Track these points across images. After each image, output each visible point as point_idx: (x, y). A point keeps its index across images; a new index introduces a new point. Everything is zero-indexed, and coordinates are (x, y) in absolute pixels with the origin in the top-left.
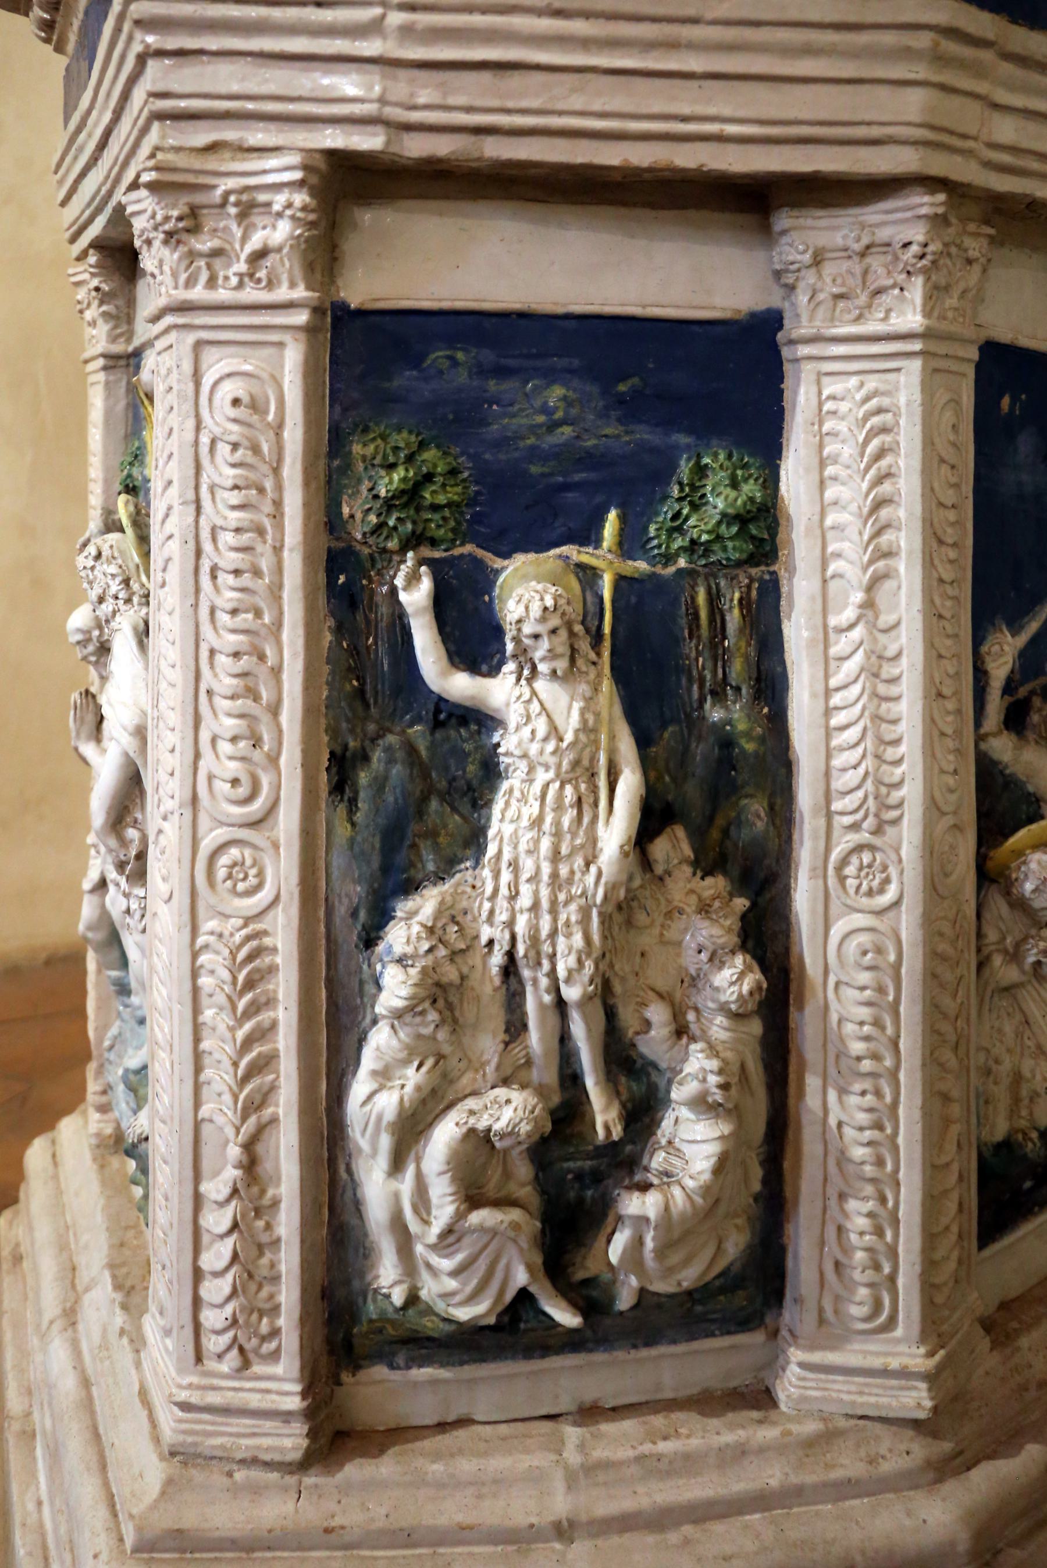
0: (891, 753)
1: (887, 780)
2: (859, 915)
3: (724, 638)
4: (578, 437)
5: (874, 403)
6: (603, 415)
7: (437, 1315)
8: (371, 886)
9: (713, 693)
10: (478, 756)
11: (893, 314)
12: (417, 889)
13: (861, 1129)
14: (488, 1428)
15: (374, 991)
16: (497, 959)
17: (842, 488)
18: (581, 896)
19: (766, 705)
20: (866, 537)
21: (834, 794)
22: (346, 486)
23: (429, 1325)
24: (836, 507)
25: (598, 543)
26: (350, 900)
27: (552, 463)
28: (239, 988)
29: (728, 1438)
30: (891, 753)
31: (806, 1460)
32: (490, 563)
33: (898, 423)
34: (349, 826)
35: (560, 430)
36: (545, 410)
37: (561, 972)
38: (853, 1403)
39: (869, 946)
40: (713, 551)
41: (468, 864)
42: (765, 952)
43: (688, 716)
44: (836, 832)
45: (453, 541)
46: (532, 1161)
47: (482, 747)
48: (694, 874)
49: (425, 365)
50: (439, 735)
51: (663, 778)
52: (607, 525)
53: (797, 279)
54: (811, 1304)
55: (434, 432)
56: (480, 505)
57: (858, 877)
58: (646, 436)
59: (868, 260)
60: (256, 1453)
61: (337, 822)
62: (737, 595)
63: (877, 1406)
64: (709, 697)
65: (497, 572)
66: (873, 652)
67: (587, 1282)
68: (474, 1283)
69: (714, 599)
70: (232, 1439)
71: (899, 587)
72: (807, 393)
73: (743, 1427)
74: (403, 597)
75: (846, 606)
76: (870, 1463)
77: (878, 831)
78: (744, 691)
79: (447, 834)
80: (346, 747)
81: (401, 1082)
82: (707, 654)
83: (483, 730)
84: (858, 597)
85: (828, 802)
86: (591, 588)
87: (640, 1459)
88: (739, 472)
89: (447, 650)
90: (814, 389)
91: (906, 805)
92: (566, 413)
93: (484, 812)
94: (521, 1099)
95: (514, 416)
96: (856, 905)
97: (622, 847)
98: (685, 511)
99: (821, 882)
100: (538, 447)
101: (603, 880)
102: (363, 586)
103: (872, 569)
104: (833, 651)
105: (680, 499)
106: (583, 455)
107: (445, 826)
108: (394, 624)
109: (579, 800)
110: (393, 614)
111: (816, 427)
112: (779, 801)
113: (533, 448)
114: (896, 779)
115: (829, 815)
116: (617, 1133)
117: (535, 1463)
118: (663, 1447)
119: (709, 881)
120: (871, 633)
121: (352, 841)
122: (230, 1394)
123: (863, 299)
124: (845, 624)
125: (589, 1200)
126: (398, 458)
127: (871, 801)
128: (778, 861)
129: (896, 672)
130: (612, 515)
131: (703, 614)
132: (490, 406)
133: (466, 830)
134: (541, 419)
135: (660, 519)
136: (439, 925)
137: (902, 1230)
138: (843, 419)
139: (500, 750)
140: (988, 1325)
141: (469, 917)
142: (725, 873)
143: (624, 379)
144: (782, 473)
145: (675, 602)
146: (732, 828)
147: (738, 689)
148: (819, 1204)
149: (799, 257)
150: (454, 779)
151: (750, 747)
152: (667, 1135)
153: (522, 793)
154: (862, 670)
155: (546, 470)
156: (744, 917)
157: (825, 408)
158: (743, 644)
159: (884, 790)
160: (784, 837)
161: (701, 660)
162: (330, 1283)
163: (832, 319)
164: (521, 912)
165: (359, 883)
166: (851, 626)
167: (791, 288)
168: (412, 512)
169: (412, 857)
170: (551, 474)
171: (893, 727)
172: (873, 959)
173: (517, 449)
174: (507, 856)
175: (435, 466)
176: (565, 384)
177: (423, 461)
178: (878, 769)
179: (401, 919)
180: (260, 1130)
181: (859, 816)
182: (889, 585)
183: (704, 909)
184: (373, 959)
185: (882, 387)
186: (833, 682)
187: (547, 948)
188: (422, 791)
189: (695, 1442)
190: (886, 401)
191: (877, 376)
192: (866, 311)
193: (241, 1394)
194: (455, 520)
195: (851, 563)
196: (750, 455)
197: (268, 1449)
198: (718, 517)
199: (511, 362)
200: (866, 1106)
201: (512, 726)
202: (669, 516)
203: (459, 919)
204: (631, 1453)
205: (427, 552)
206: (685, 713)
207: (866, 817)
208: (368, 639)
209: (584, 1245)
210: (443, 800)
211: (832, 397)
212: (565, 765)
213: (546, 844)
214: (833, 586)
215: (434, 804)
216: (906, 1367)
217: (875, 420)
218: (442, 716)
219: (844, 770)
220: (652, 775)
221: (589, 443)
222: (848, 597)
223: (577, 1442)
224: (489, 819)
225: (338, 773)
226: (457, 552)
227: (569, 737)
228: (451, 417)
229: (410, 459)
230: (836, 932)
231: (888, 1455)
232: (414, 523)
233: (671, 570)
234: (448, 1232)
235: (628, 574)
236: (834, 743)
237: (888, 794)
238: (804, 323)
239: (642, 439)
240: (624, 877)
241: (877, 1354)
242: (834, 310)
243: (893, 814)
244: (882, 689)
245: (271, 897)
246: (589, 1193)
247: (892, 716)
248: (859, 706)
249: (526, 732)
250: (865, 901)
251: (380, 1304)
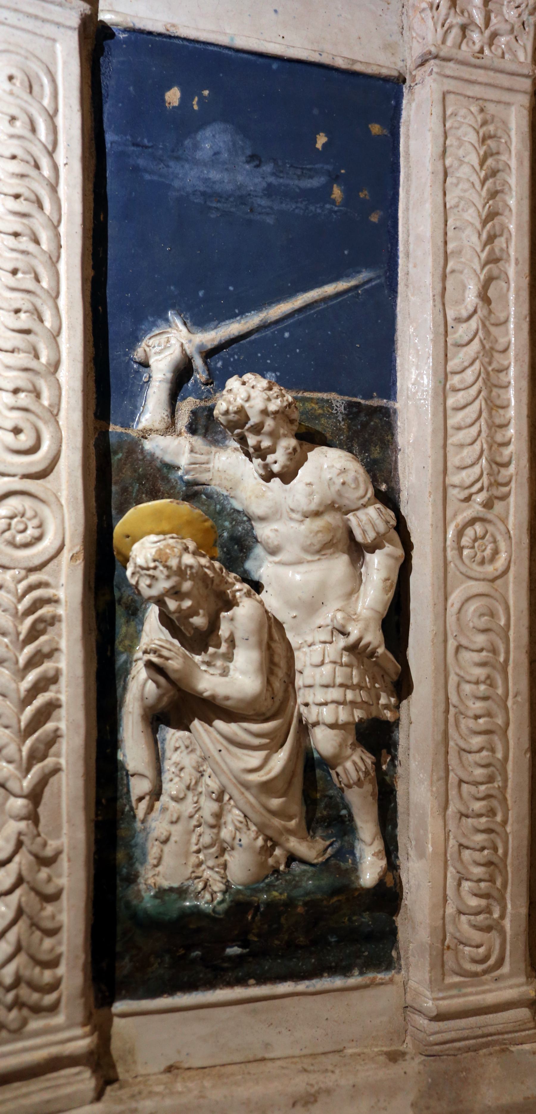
1: (498, 459)
28: (22, 637)
57: (473, 547)
77: (488, 505)
114: (506, 459)
127: (485, 478)
140: (386, 1110)
180: (43, 782)
230: (455, 598)
250: (478, 570)
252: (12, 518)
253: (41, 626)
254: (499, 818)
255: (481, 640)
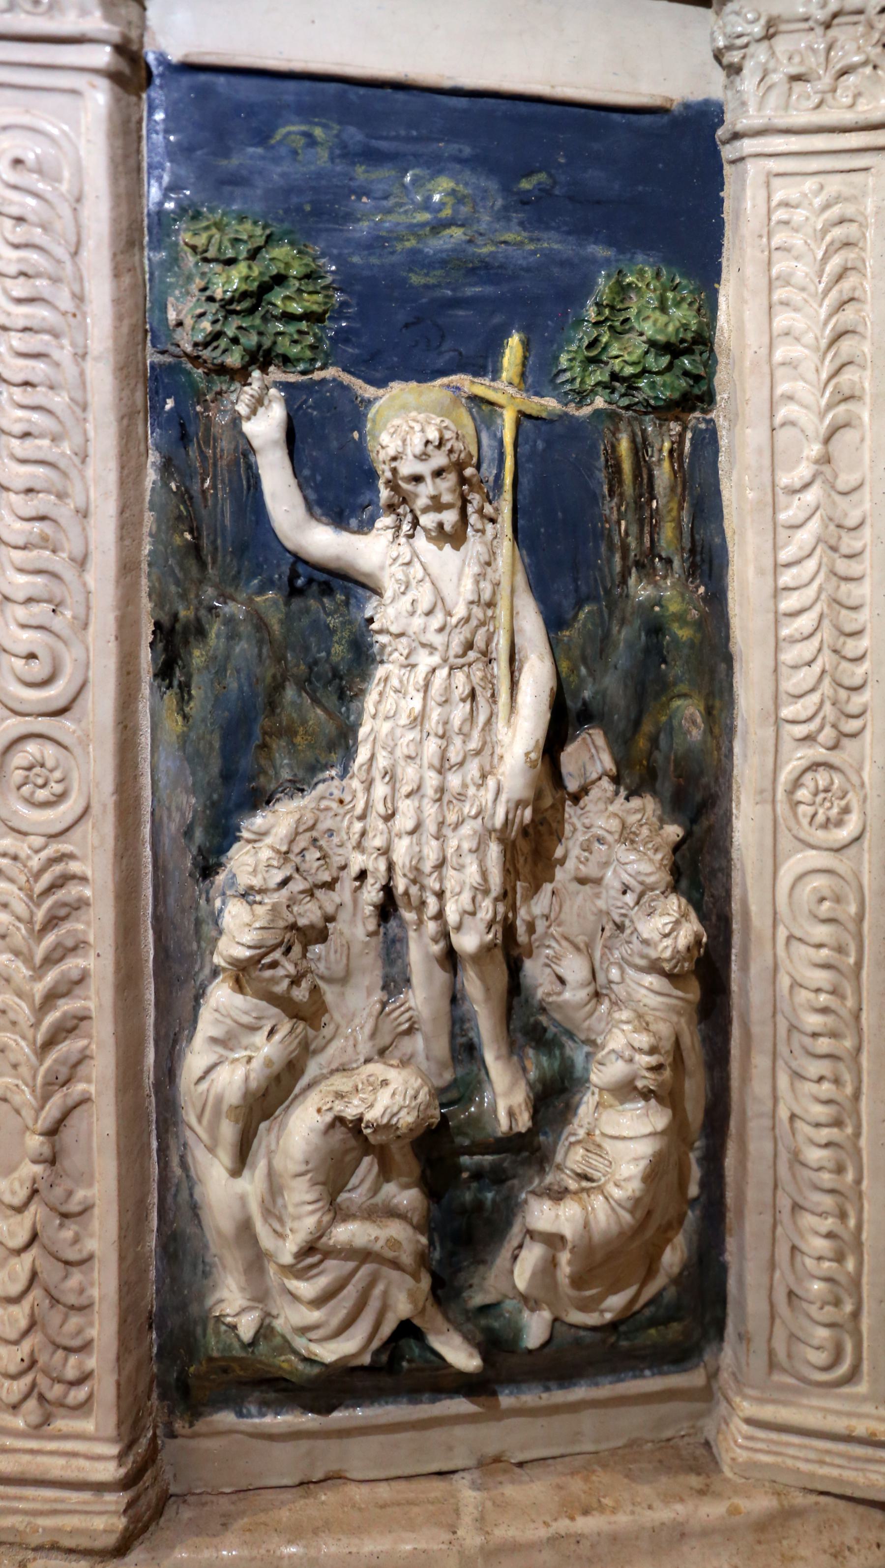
0: (852, 647)
1: (847, 682)
2: (814, 852)
3: (652, 497)
4: (470, 241)
5: (835, 212)
6: (503, 215)
7: (295, 1352)
8: (210, 797)
9: (639, 565)
10: (346, 634)
11: (862, 100)
12: (268, 802)
13: (818, 1125)
14: (365, 1489)
15: (214, 933)
16: (372, 894)
17: (793, 315)
18: (475, 817)
19: (702, 583)
20: (824, 376)
21: (783, 697)
22: (171, 286)
23: (287, 1363)
24: (789, 339)
25: (496, 374)
26: (183, 815)
27: (438, 273)
29: (664, 1514)
30: (852, 647)
31: (758, 1548)
32: (360, 392)
33: (864, 236)
34: (180, 719)
35: (448, 232)
36: (427, 205)
37: (452, 915)
38: (812, 1475)
39: (826, 893)
40: (638, 389)
41: (333, 773)
42: (703, 895)
43: (608, 592)
44: (787, 745)
45: (313, 360)
46: (416, 1155)
47: (350, 622)
48: (617, 793)
49: (273, 142)
50: (297, 603)
51: (579, 670)
52: (507, 351)
53: (744, 58)
54: (759, 1345)
55: (286, 226)
56: (347, 319)
57: (813, 804)
58: (556, 246)
59: (833, 33)
60: (56, 1538)
61: (164, 714)
62: (667, 445)
63: (839, 1481)
64: (634, 570)
65: (369, 403)
66: (831, 519)
67: (485, 1309)
68: (342, 1313)
69: (640, 448)
70: (27, 1519)
71: (862, 440)
72: (754, 198)
73: (682, 1500)
74: (248, 427)
75: (798, 461)
76: (835, 1556)
78: (676, 564)
79: (306, 733)
80: (175, 617)
81: (248, 1053)
82: (630, 515)
83: (353, 601)
84: (815, 449)
85: (777, 707)
86: (488, 428)
87: (555, 1540)
88: (670, 295)
89: (305, 498)
90: (763, 193)
91: (868, 715)
92: (455, 211)
93: (353, 706)
94: (400, 1080)
95: (389, 211)
96: (811, 840)
97: (527, 754)
98: (604, 339)
99: (769, 808)
100: (420, 251)
101: (503, 797)
102: (197, 413)
103: (830, 416)
104: (782, 517)
105: (597, 324)
106: (477, 264)
107: (304, 722)
108: (237, 463)
109: (473, 695)
110: (236, 448)
111: (765, 240)
112: (717, 704)
113: (414, 252)
114: (857, 681)
115: (778, 721)
116: (524, 1122)
117: (423, 1545)
118: (585, 1524)
119: (636, 802)
120: (829, 496)
121: (184, 739)
122: (27, 1458)
123: (827, 80)
124: (798, 484)
125: (489, 1203)
126: (238, 253)
127: (828, 708)
128: (717, 779)
129: (857, 545)
130: (514, 343)
131: (627, 466)
132: (359, 198)
133: (330, 728)
134: (426, 216)
135: (574, 347)
136: (296, 849)
137: (866, 1257)
138: (796, 230)
139: (374, 626)
141: (335, 840)
142: (655, 793)
143: (528, 174)
144: (722, 300)
145: (592, 451)
146: (662, 736)
147: (669, 562)
148: (768, 1218)
149: (748, 29)
150: (316, 662)
151: (684, 633)
152: (585, 1122)
153: (401, 681)
154: (819, 540)
155: (431, 281)
156: (677, 848)
157: (775, 217)
158: (674, 505)
159: (843, 694)
160: (724, 750)
161: (623, 523)
162: (161, 1308)
163: (787, 107)
164: (399, 836)
165: (194, 793)
166: (806, 486)
167: (734, 70)
168: (258, 322)
169: (263, 762)
170: (438, 286)
171: (853, 615)
172: (830, 909)
173: (393, 253)
174: (382, 761)
175: (288, 265)
176: (453, 176)
177: (272, 259)
178: (836, 668)
179: (249, 841)
181: (813, 726)
182: (847, 437)
183: (627, 835)
184: (212, 892)
185: (847, 191)
186: (784, 556)
187: (433, 883)
188: (274, 677)
189: (622, 1519)
190: (849, 210)
191: (839, 177)
192: (829, 96)
193: (41, 1459)
194: (315, 335)
195: (806, 407)
196: (683, 275)
197: (73, 1532)
198: (645, 347)
199: (383, 145)
200: (824, 1096)
201: (388, 594)
202: (586, 343)
203: (322, 842)
204: (543, 1533)
205: (275, 374)
206: (605, 589)
207: (821, 728)
208: (203, 481)
209: (483, 1262)
210: (301, 688)
211: (786, 204)
212: (456, 647)
213: (432, 747)
214: (783, 435)
215: (290, 693)
216: (874, 1434)
217: (837, 232)
218: (300, 582)
219: (795, 667)
220: (564, 666)
221: (485, 250)
222: (801, 451)
223: (476, 1514)
224: (360, 713)
225: (166, 649)
226: (317, 376)
227: (460, 611)
228: (308, 208)
229: (253, 255)
231: (856, 1547)
232: (260, 334)
233: (586, 411)
234: (309, 1249)
235: (534, 413)
236: (784, 632)
237: (848, 701)
238: (751, 111)
239: (551, 249)
240: (528, 794)
241: (838, 1413)
242: (790, 96)
243: (852, 726)
244: (842, 566)
245: (79, 810)
246: (490, 1195)
247: (852, 602)
248: (815, 585)
249: (404, 603)
250: (820, 836)
251: (223, 1337)
252: (29, 769)
253: (62, 912)
254: (850, 1176)
255: (822, 932)
